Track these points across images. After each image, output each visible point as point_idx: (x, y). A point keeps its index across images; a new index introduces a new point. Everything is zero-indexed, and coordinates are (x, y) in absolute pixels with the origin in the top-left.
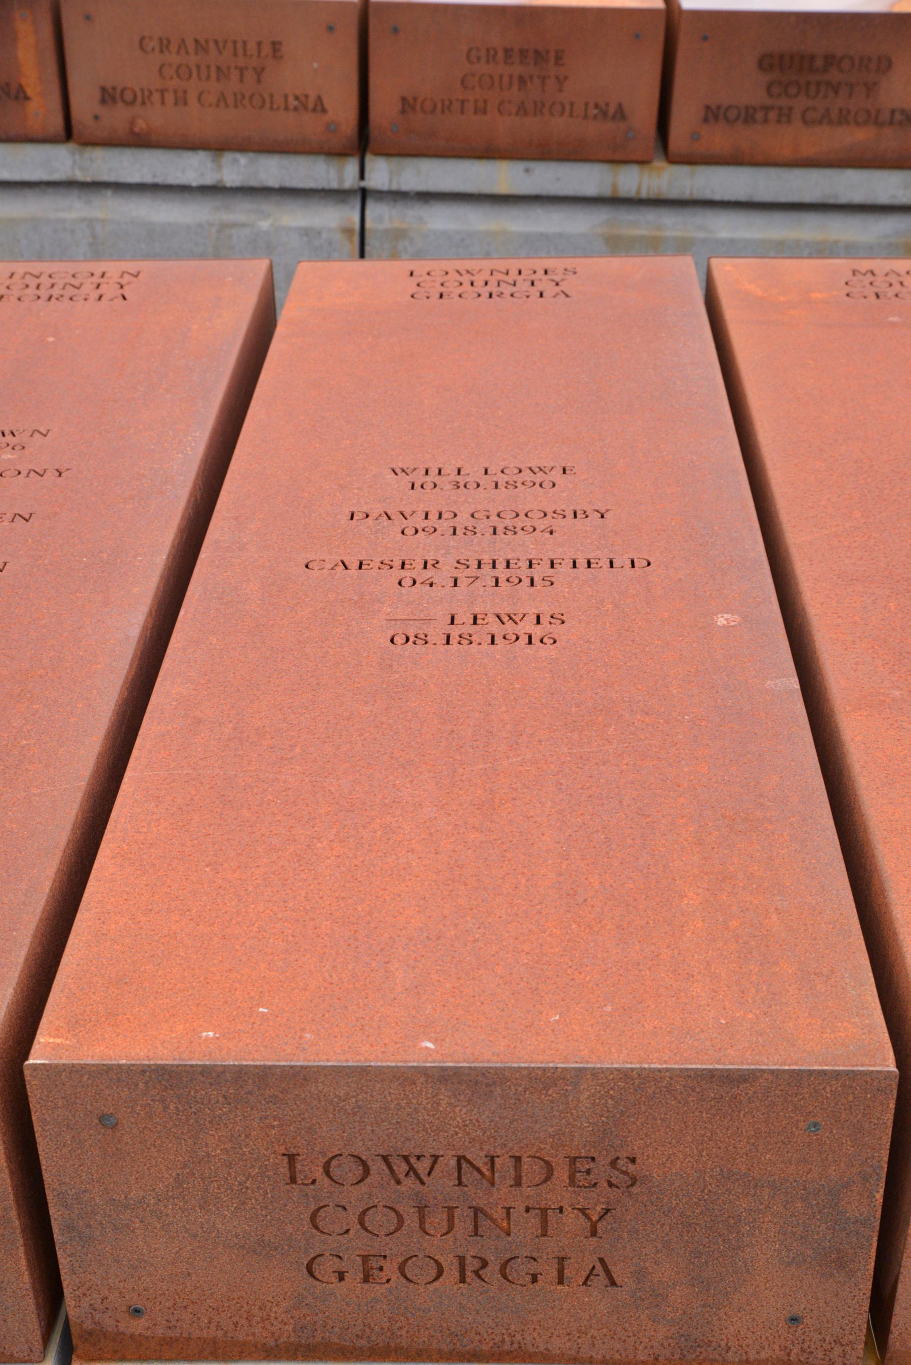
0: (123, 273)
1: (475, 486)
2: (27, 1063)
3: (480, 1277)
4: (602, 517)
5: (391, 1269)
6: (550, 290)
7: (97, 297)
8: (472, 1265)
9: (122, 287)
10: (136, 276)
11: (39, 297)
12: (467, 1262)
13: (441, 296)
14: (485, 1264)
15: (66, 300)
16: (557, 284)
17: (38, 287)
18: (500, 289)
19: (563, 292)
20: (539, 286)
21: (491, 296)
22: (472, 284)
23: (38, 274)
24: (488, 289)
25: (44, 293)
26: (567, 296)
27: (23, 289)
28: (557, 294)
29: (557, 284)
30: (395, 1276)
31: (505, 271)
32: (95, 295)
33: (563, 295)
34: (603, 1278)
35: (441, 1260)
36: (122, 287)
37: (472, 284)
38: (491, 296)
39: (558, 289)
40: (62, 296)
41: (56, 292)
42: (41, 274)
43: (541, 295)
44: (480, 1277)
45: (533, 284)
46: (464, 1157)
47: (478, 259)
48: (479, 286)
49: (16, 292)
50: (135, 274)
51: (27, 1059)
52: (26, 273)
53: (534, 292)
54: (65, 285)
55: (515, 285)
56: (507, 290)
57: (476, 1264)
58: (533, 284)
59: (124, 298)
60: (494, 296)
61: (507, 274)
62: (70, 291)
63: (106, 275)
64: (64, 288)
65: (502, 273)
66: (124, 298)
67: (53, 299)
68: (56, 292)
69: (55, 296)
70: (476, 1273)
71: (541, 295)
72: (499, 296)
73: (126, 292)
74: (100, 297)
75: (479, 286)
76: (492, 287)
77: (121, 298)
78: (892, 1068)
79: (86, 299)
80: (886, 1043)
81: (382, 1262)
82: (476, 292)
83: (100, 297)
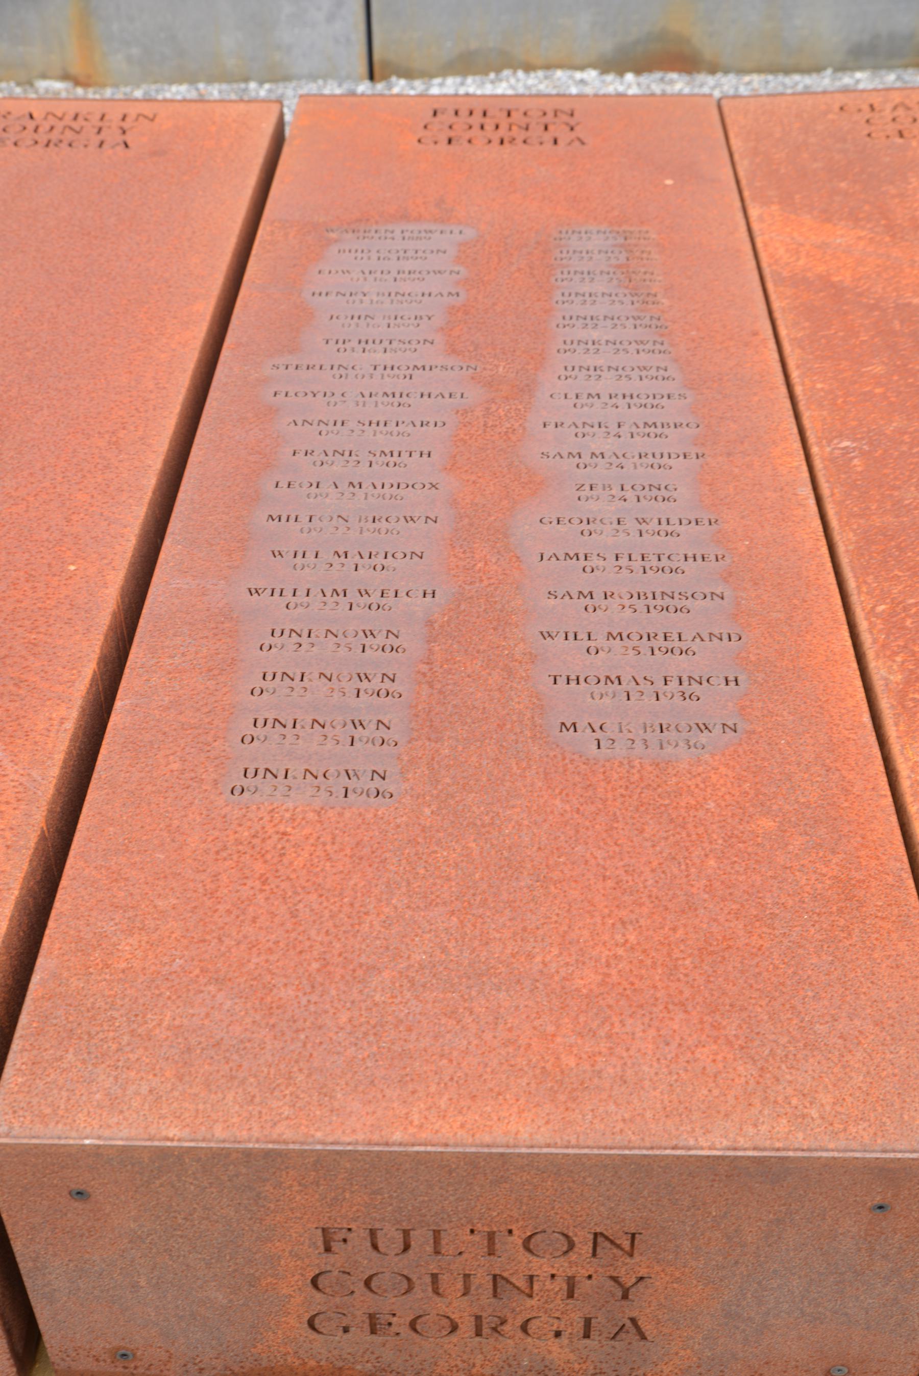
0: (48, 114)
1: (403, 556)
4: (625, 1296)
6: (565, 136)
7: (98, 143)
9: (124, 132)
10: (152, 120)
11: (36, 142)
13: (450, 141)
15: (64, 145)
17: (36, 130)
19: (579, 139)
20: (553, 131)
23: (151, 116)
25: (42, 137)
27: (21, 132)
28: (572, 141)
29: (572, 129)
32: (96, 140)
36: (124, 132)
38: (502, 142)
39: (573, 135)
40: (61, 141)
41: (55, 136)
42: (64, 114)
43: (555, 142)
45: (546, 128)
49: (11, 137)
50: (151, 116)
52: (139, 115)
53: (548, 137)
54: (65, 127)
55: (527, 129)
56: (521, 135)
58: (546, 128)
59: (126, 145)
61: (572, 115)
62: (69, 135)
63: (106, 118)
66: (126, 145)
67: (51, 145)
68: (55, 136)
72: (510, 142)
73: (129, 138)
74: (101, 144)
77: (123, 146)
79: (86, 146)
80: (831, 584)
83: (101, 144)
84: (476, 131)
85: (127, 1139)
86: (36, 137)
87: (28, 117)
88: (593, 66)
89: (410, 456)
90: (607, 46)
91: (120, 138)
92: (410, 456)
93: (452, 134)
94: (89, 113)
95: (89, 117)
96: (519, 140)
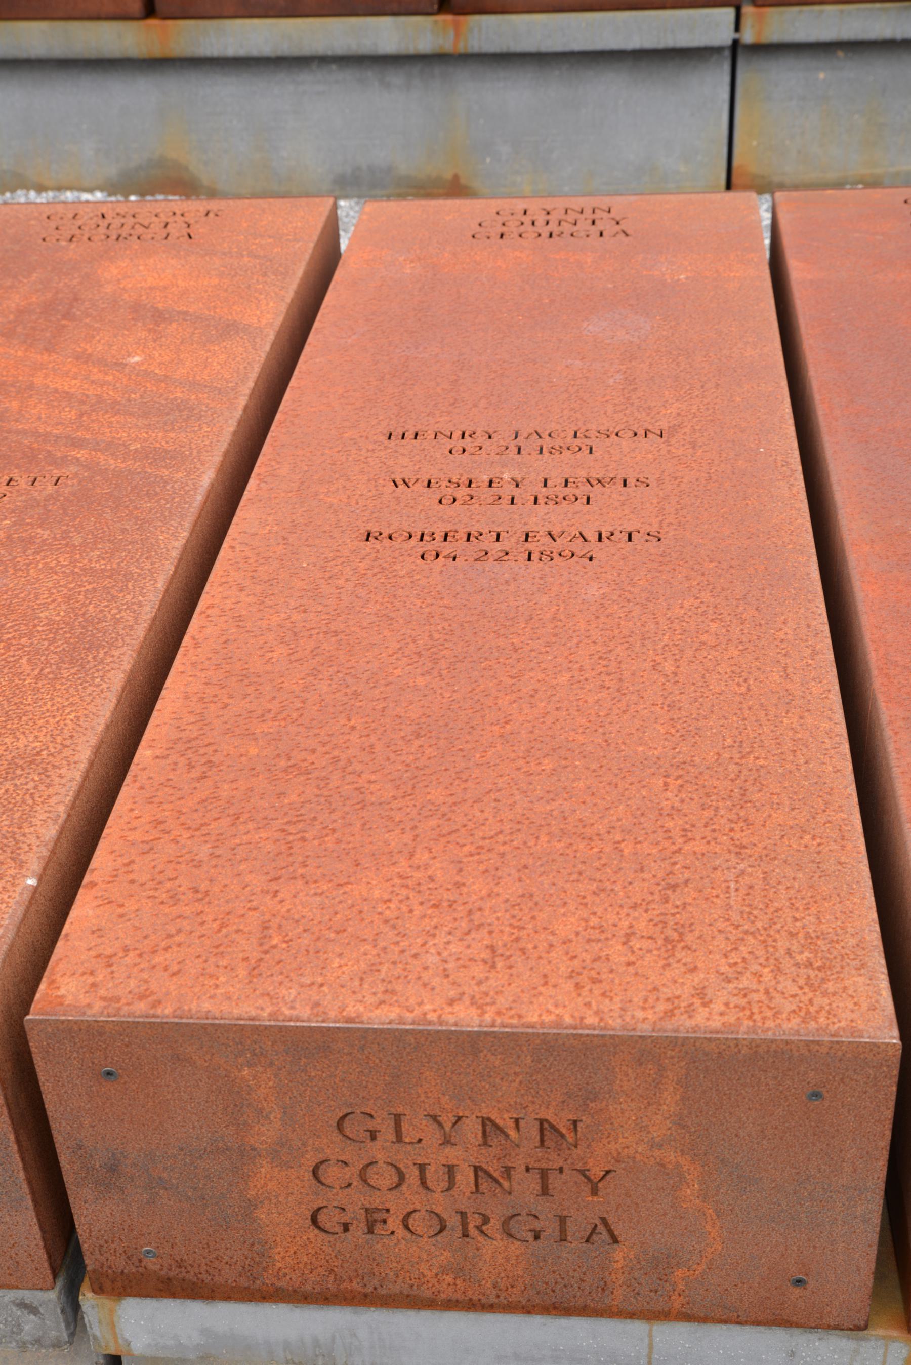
2: (28, 1017)
3: (482, 1232)
5: (394, 1223)
8: (474, 1221)
9: (189, 226)
12: (470, 1219)
13: (502, 236)
14: (486, 1220)
16: (618, 223)
18: (561, 229)
19: (624, 232)
20: (600, 226)
21: (551, 236)
22: (533, 224)
24: (106, 222)
26: (627, 235)
29: (618, 223)
30: (401, 1232)
31: (580, 210)
33: (623, 235)
34: (605, 1236)
35: (445, 1216)
37: (533, 224)
38: (551, 236)
39: (618, 228)
43: (601, 235)
44: (482, 1232)
45: (593, 223)
46: (489, 1119)
47: (542, 197)
48: (540, 226)
51: (27, 1013)
53: (594, 231)
57: (479, 1221)
58: (593, 223)
59: (190, 237)
60: (554, 235)
61: (582, 212)
62: (139, 230)
64: (133, 228)
65: (604, 210)
66: (190, 237)
67: (121, 239)
69: (124, 235)
70: (478, 1228)
71: (601, 235)
72: (559, 236)
75: (540, 226)
76: (553, 227)
78: (891, 1036)
81: (385, 1215)
82: (535, 232)
84: (528, 226)
85: (53, 968)
86: (108, 233)
87: (100, 216)
88: (101, 190)
89: (630, 539)
90: (112, 171)
91: (185, 232)
92: (630, 539)
93: (504, 229)
94: (219, 210)
95: (219, 213)
96: (567, 235)
